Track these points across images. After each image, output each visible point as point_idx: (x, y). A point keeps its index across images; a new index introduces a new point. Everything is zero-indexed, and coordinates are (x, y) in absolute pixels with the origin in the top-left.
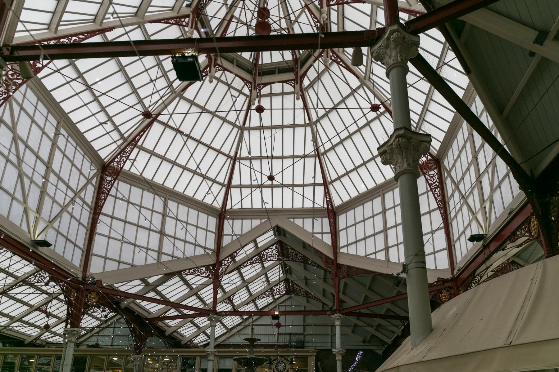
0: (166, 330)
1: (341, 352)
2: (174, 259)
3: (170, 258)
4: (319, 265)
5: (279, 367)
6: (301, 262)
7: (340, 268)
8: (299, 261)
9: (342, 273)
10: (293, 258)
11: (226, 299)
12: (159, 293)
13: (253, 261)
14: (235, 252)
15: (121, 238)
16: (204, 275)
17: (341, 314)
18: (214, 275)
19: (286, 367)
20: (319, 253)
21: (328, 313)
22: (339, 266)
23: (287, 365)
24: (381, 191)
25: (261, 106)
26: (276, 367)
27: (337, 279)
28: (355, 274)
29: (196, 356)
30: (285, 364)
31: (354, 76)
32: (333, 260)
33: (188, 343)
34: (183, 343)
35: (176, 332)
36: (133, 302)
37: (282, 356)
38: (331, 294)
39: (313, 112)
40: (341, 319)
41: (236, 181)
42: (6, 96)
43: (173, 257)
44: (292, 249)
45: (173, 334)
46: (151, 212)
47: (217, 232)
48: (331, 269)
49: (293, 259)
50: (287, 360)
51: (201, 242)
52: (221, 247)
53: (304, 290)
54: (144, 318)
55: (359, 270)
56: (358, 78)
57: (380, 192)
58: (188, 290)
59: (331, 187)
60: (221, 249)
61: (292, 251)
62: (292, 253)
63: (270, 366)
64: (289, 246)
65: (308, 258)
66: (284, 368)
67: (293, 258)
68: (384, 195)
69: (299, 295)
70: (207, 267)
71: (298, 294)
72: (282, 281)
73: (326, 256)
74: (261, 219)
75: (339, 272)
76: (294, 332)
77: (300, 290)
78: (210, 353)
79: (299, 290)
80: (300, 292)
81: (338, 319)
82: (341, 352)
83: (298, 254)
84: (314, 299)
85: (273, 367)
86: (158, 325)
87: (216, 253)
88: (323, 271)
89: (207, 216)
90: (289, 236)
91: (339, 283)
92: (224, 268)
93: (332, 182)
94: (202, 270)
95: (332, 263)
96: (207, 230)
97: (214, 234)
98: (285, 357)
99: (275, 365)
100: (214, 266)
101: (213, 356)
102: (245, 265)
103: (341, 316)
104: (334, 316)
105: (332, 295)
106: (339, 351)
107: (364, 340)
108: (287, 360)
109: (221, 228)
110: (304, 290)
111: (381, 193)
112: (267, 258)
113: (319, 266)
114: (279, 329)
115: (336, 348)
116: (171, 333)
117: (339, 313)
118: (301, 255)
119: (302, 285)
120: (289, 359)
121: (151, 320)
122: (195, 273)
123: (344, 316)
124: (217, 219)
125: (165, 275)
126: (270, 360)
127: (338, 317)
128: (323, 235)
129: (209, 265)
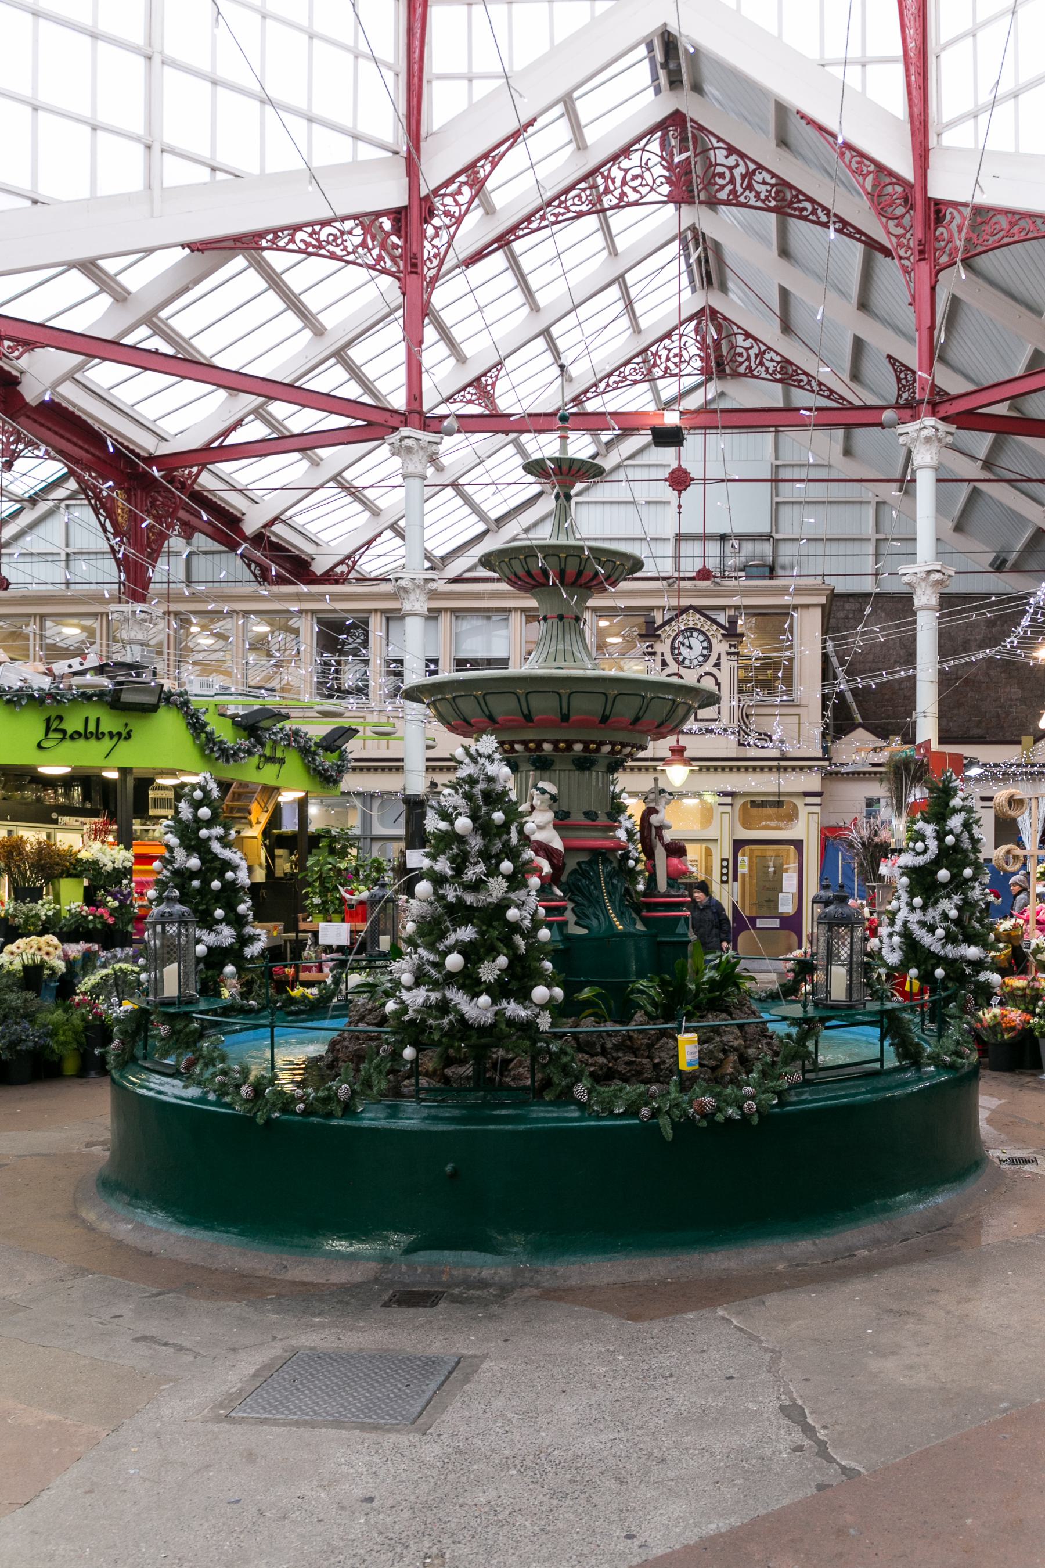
0: (243, 514)
1: (937, 576)
2: (220, 176)
3: (203, 174)
4: (845, 223)
5: (684, 651)
6: (769, 209)
7: (939, 219)
8: (759, 204)
9: (949, 242)
10: (734, 192)
11: (470, 385)
12: (169, 336)
14: (486, 156)
15: (283, 517)
17: (942, 419)
18: (400, 257)
19: (709, 648)
20: (848, 155)
21: (888, 415)
22: (938, 212)
23: (714, 641)
26: (673, 648)
27: (925, 268)
28: (1006, 240)
29: (370, 611)
30: (707, 639)
32: (912, 186)
33: (338, 570)
34: (319, 567)
35: (284, 521)
36: (70, 376)
37: (699, 610)
38: (886, 361)
40: (940, 440)
43: (214, 169)
44: (731, 150)
45: (274, 528)
49: (737, 197)
50: (714, 621)
52: (423, 133)
53: (778, 354)
54: (138, 456)
58: (308, 334)
60: (423, 144)
61: (732, 161)
63: (651, 646)
64: (719, 140)
65: (800, 192)
66: (704, 656)
67: (734, 192)
69: (757, 377)
70: (367, 220)
71: (751, 371)
72: (690, 319)
73: (881, 168)
75: (937, 239)
76: (738, 529)
77: (761, 354)
78: (410, 585)
79: (756, 356)
80: (761, 364)
81: (928, 440)
83: (754, 172)
85: (663, 648)
86: (200, 485)
87: (403, 162)
88: (860, 247)
90: (716, 93)
91: (933, 289)
95: (906, 200)
98: (708, 613)
99: (669, 642)
100: (398, 215)
101: (423, 598)
102: (534, 226)
103: (942, 426)
104: (911, 427)
105: (893, 365)
106: (929, 572)
107: (996, 558)
108: (714, 621)
109: (418, 25)
110: (778, 354)
113: (845, 228)
114: (684, 493)
115: (914, 562)
116: (264, 526)
117: (933, 414)
118: (768, 178)
119: (769, 332)
120: (722, 618)
121: (171, 462)
123: (952, 428)
125: (196, 247)
126: (650, 622)
127: (925, 433)
129: (379, 214)
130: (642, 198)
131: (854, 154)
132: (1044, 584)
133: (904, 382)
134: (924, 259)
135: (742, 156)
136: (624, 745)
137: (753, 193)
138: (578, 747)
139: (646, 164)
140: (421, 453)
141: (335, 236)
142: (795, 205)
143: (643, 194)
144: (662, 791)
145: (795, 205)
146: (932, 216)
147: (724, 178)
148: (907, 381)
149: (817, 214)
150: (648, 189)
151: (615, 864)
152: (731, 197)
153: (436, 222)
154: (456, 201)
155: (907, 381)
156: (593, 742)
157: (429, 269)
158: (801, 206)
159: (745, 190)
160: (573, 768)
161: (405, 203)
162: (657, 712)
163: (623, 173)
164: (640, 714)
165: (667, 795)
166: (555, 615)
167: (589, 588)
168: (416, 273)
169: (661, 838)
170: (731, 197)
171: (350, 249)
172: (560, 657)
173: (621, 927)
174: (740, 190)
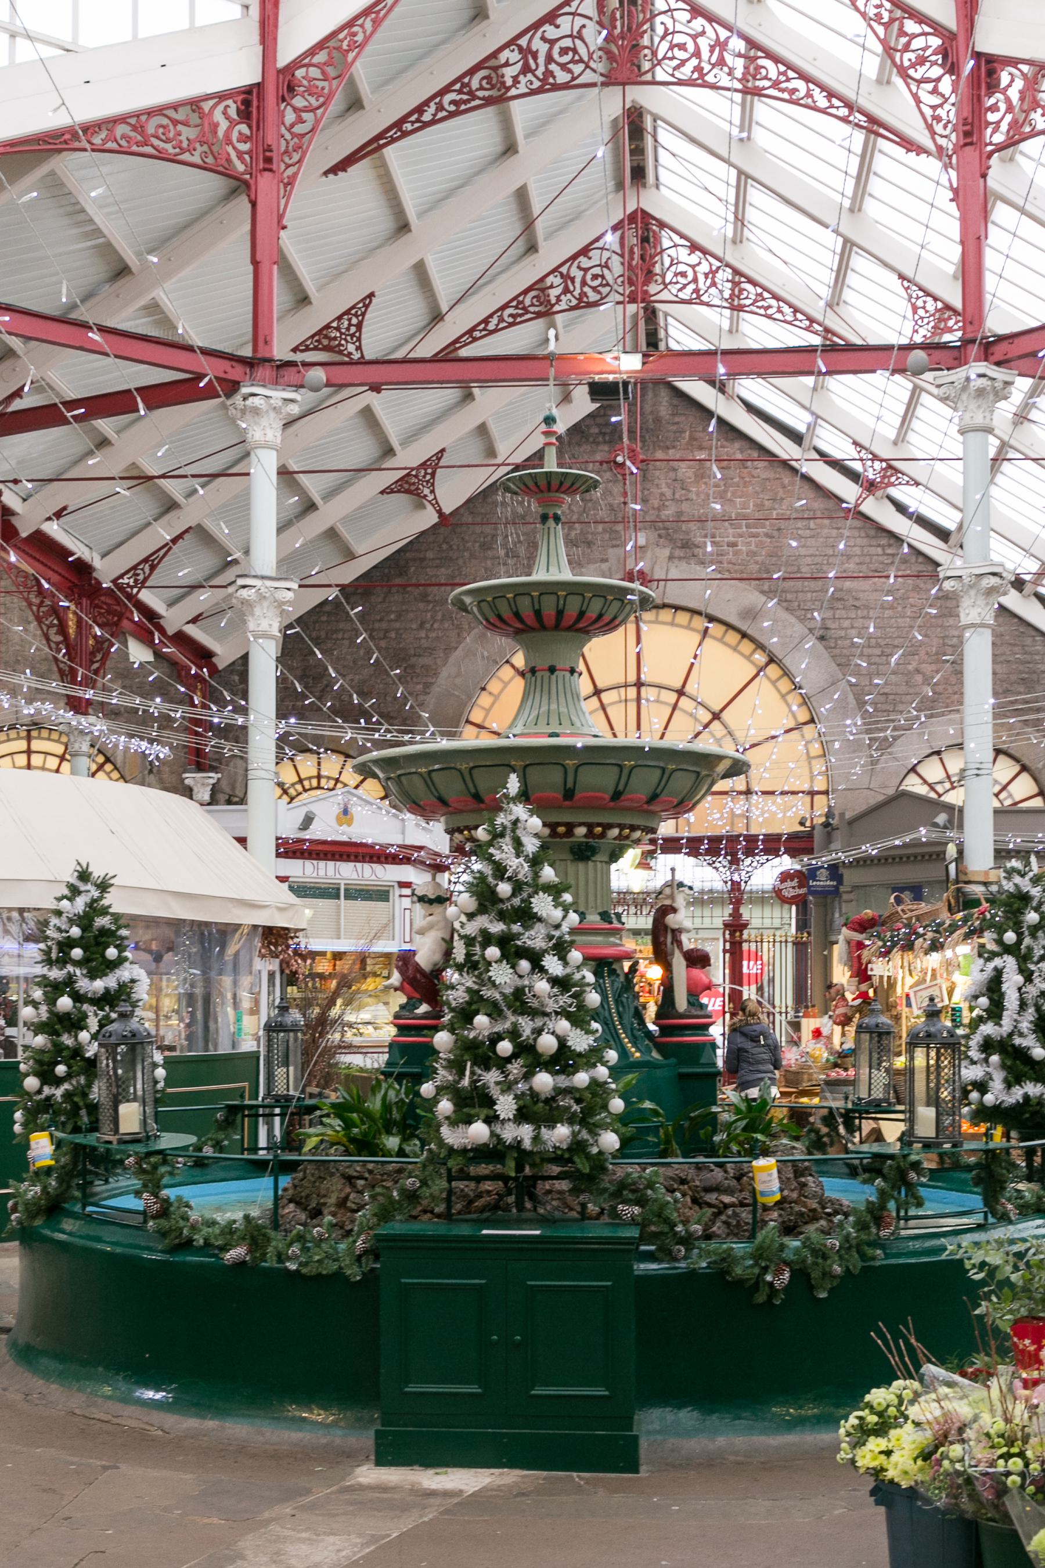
10: (698, 69)
13: (471, 93)
16: (197, 153)
42: (171, 151)
44: (694, 247)
48: (935, 91)
49: (702, 75)
56: (822, 454)
62: (693, 267)
67: (698, 69)
83: (717, 270)
84: (823, 111)
92: (306, 110)
94: (185, 124)
95: (291, 89)
112: (583, 294)
130: (574, 79)
132: (660, 5)
134: (971, 144)
136: (633, 828)
137: (726, 69)
138: (581, 831)
139: (579, 32)
141: (164, 127)
142: (783, 85)
143: (576, 73)
144: (681, 885)
145: (783, 85)
147: (686, 50)
149: (811, 96)
150: (581, 66)
151: (622, 979)
152: (696, 75)
153: (299, 102)
154: (323, 73)
155: (350, 320)
156: (599, 825)
157: (288, 166)
159: (714, 66)
160: (570, 857)
161: (258, 79)
162: (642, 784)
163: (547, 46)
164: (658, 791)
165: (686, 889)
166: (546, 666)
167: (587, 632)
168: (271, 170)
169: (679, 944)
171: (185, 145)
172: (554, 720)
173: (638, 1054)
174: (707, 67)
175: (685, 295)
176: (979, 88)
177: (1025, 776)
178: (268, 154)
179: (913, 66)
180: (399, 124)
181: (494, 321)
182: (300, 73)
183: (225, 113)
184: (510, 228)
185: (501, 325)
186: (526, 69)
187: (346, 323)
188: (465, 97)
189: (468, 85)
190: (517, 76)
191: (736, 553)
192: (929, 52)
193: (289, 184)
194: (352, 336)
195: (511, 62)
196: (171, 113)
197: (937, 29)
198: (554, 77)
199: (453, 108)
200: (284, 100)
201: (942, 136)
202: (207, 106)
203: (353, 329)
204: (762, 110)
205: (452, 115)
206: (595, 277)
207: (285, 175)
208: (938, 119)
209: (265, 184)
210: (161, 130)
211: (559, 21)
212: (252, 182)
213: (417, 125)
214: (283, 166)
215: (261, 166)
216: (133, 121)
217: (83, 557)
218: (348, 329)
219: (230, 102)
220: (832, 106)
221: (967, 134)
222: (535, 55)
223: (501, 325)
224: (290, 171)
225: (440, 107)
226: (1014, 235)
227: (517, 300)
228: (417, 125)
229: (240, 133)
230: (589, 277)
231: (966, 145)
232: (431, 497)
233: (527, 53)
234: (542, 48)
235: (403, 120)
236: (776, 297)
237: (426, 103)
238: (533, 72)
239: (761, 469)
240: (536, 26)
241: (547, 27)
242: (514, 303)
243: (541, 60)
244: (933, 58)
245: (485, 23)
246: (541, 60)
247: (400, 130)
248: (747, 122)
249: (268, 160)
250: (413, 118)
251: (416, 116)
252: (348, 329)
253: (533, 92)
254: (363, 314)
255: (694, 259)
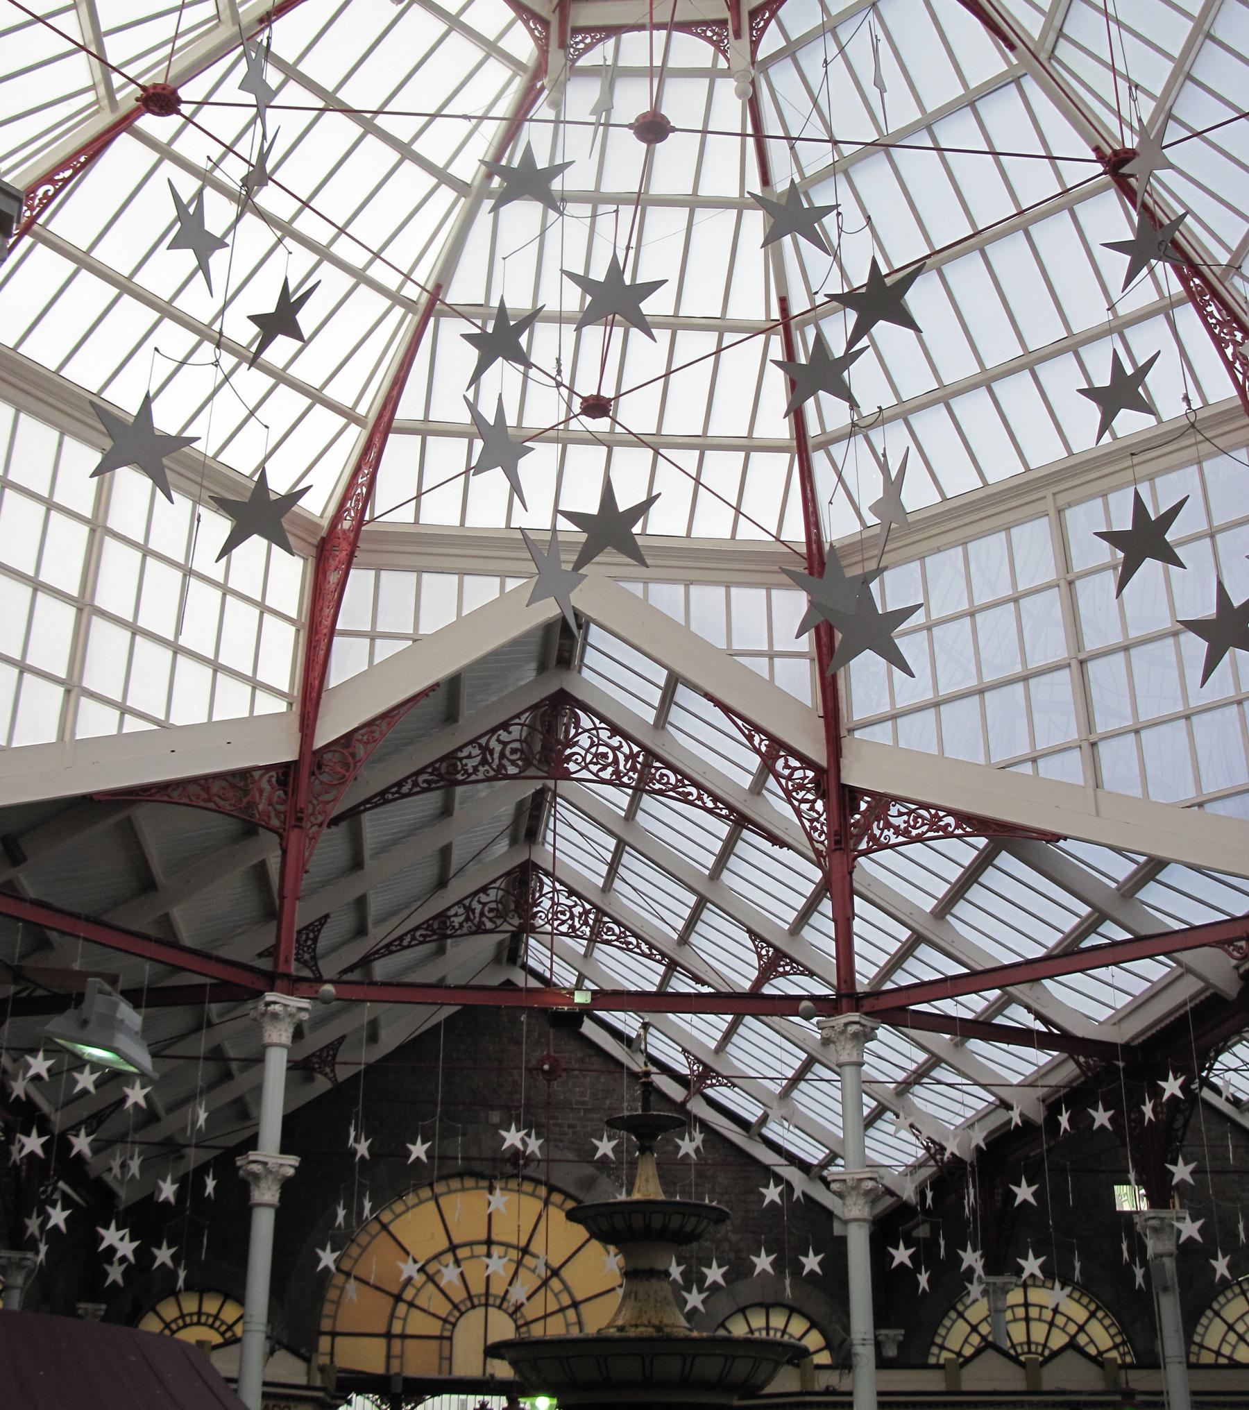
1: (854, 1028)
10: (572, 927)
17: (867, 1014)
24: (1050, 497)
25: (663, 117)
31: (976, 21)
38: (324, 913)
39: (778, 151)
41: (409, 408)
46: (42, 509)
47: (305, 619)
51: (237, 656)
52: (324, 689)
55: (193, 789)
57: (1045, 497)
59: (819, 461)
68: (1060, 512)
74: (503, 576)
82: (854, 1028)
89: (55, 434)
93: (826, 443)
95: (319, 767)
96: (263, 608)
97: (293, 629)
111: (1049, 504)
122: (210, 800)
124: (305, 560)
128: (378, 642)
131: (763, 737)
133: (311, 935)
134: (840, 849)
135: (580, 897)
140: (288, 1020)
141: (224, 788)
142: (680, 790)
145: (680, 790)
146: (291, 780)
148: (307, 934)
152: (614, 777)
153: (325, 778)
155: (307, 934)
158: (686, 790)
159: (582, 925)
168: (300, 827)
170: (614, 777)
175: (564, 928)
176: (845, 809)
177: (748, 1313)
178: (300, 815)
179: (795, 790)
180: (382, 794)
181: (408, 938)
182: (328, 756)
183: (269, 781)
184: (429, 873)
185: (413, 943)
186: (484, 762)
187: (304, 937)
188: (435, 778)
189: (438, 769)
190: (477, 766)
191: (575, 1134)
192: (806, 781)
193: (313, 838)
194: (309, 947)
195: (473, 755)
196: (229, 778)
197: (807, 763)
198: (506, 770)
199: (425, 785)
200: (313, 774)
201: (818, 842)
202: (257, 774)
203: (309, 943)
204: (647, 801)
205: (424, 790)
206: (491, 910)
207: (311, 831)
208: (815, 829)
209: (294, 836)
210: (222, 791)
211: (511, 728)
212: (285, 834)
213: (396, 795)
214: (309, 825)
215: (293, 823)
216: (202, 782)
217: (931, 1176)
218: (306, 941)
219: (273, 773)
220: (717, 808)
221: (837, 842)
222: (492, 752)
223: (413, 943)
224: (315, 829)
225: (415, 784)
226: (24, 668)
227: (427, 924)
228: (396, 795)
229: (279, 797)
230: (486, 909)
231: (836, 850)
232: (331, 1075)
233: (486, 749)
234: (498, 748)
235: (386, 791)
236: (635, 935)
237: (405, 780)
238: (490, 765)
239: (597, 1063)
240: (494, 731)
241: (501, 732)
242: (425, 926)
243: (496, 755)
244: (809, 786)
245: (454, 726)
246: (496, 755)
247: (383, 798)
248: (634, 805)
249: (300, 819)
250: (394, 790)
251: (395, 789)
252: (306, 941)
253: (488, 779)
254: (319, 931)
255: (615, 741)
